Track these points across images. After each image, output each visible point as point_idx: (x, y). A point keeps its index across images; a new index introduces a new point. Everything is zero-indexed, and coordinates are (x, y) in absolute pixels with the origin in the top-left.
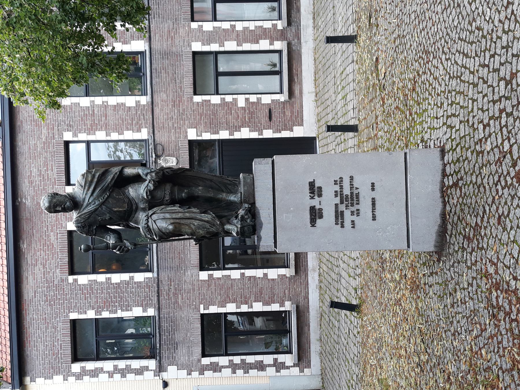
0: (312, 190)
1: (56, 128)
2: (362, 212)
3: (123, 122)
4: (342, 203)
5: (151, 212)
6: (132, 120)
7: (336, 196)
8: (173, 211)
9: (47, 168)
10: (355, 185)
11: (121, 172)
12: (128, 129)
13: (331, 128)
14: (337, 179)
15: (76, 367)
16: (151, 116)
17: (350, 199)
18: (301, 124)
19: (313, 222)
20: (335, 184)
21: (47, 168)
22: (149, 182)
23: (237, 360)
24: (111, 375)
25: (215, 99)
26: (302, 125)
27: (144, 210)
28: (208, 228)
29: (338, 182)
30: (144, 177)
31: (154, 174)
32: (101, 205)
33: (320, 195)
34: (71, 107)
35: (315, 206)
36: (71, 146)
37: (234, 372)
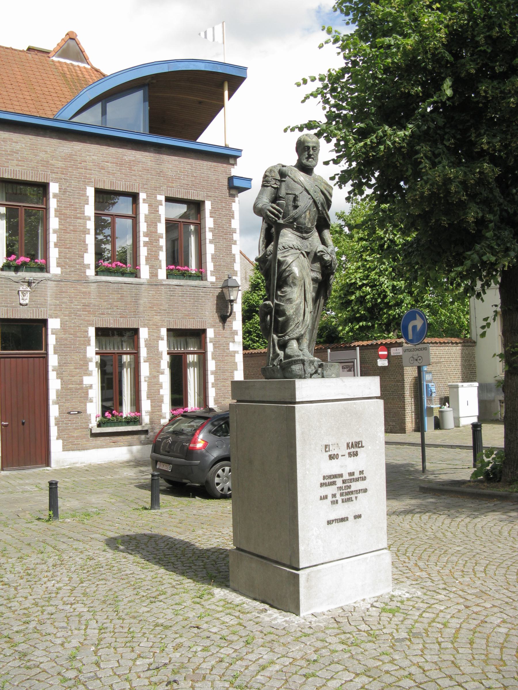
0: (356, 445)
3: (69, 248)
6: (70, 259)
9: (20, 161)
12: (60, 253)
13: (53, 487)
17: (347, 491)
18: (65, 448)
21: (20, 161)
26: (64, 450)
29: (361, 476)
34: (84, 195)
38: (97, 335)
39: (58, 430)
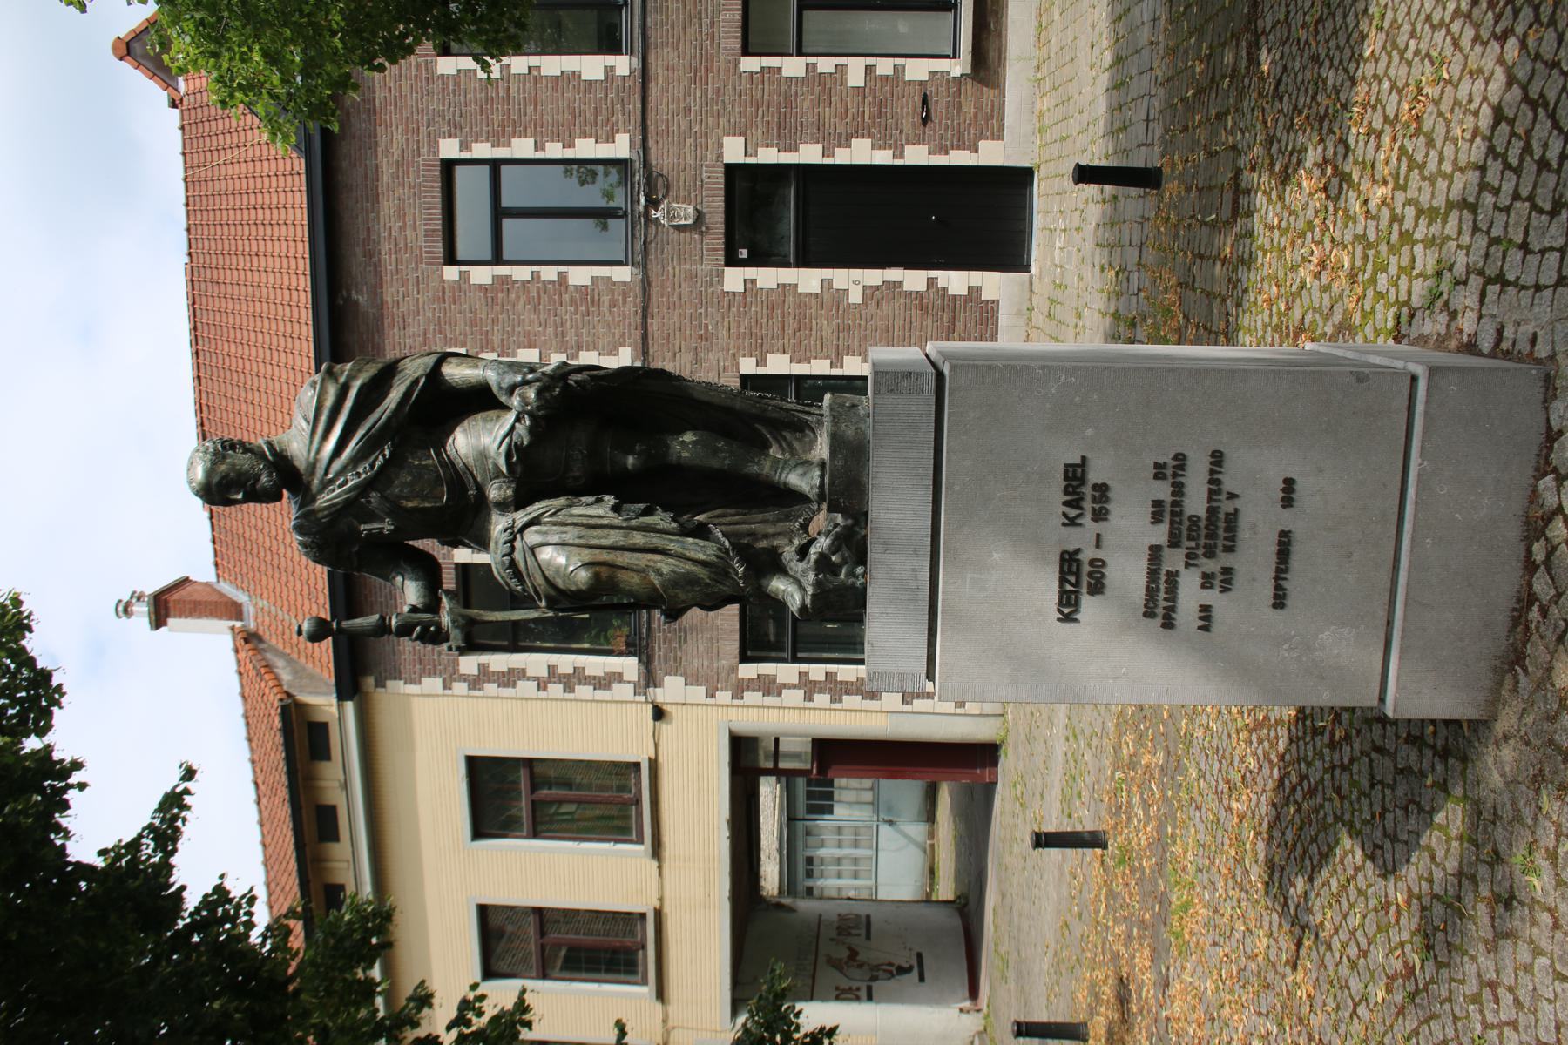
1: (423, 129)
2: (1239, 580)
4: (1174, 542)
5: (521, 517)
7: (1157, 518)
8: (592, 521)
10: (1229, 484)
11: (435, 374)
12: (584, 135)
14: (1167, 458)
15: (469, 664)
16: (639, 106)
17: (1203, 532)
19: (1068, 605)
20: (1156, 477)
22: (518, 419)
23: (817, 671)
24: (542, 685)
25: (793, 66)
26: (1000, 137)
27: (503, 506)
28: (707, 585)
30: (503, 399)
31: (532, 394)
32: (364, 488)
33: (1100, 515)
35: (1078, 551)
36: (459, 171)
37: (809, 697)
38: (760, 258)
39: (958, 148)
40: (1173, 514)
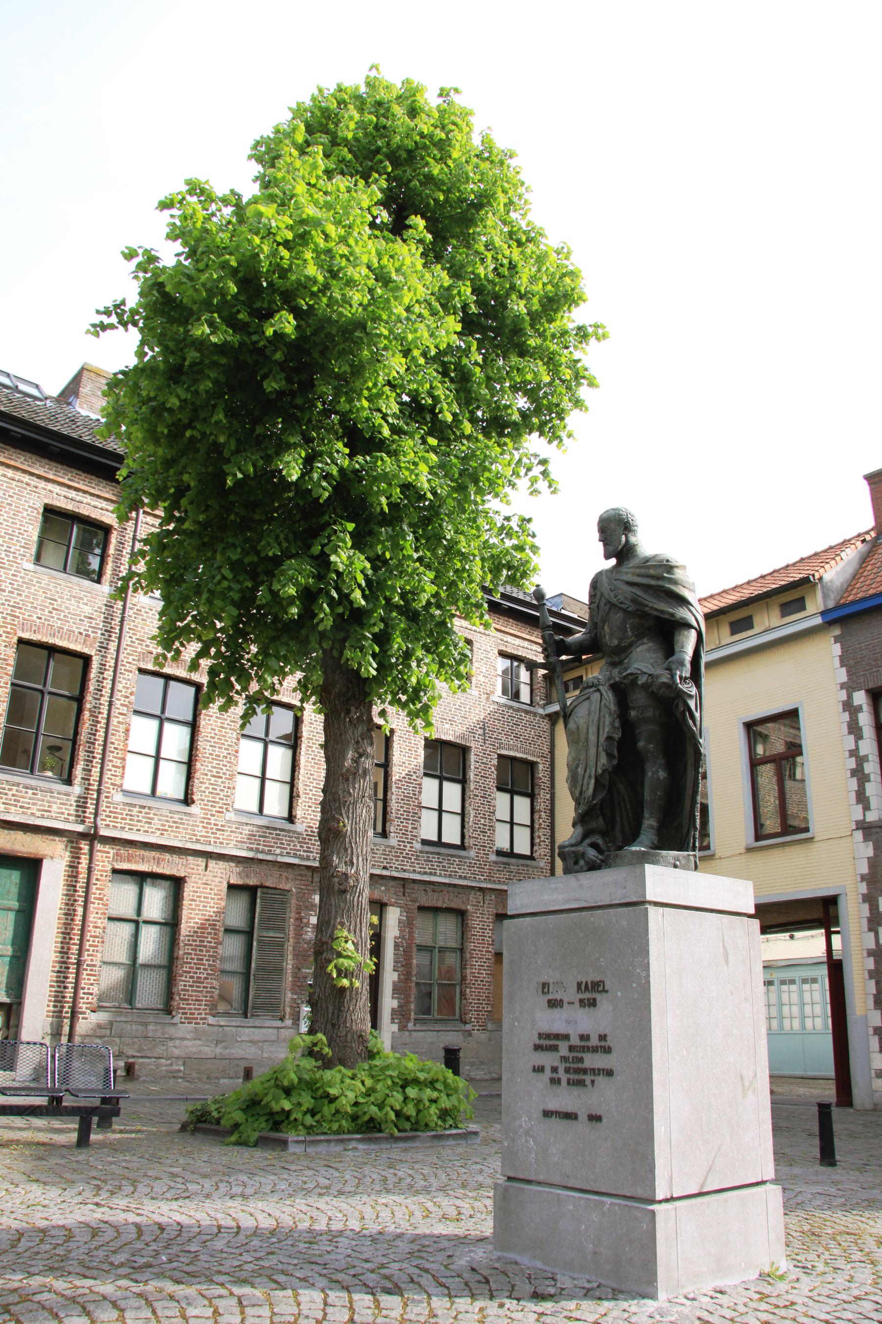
0: (593, 987)
4: (571, 1048)
15: (860, 698)
24: (854, 753)
29: (603, 1043)
40: (583, 1047)
